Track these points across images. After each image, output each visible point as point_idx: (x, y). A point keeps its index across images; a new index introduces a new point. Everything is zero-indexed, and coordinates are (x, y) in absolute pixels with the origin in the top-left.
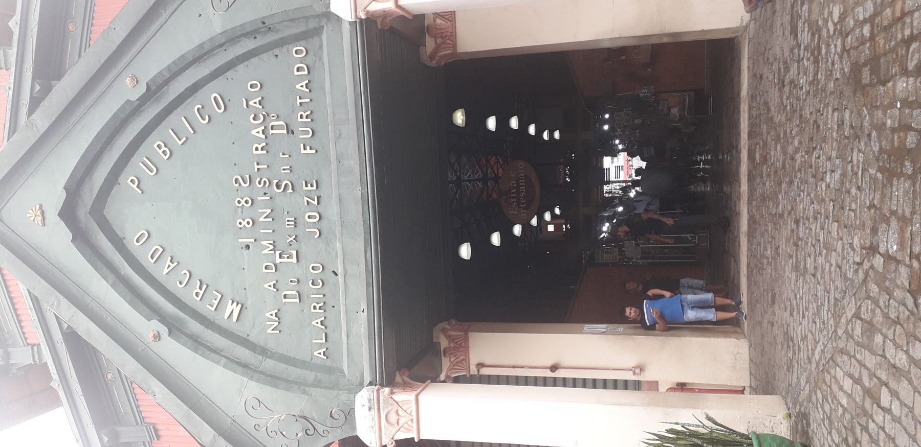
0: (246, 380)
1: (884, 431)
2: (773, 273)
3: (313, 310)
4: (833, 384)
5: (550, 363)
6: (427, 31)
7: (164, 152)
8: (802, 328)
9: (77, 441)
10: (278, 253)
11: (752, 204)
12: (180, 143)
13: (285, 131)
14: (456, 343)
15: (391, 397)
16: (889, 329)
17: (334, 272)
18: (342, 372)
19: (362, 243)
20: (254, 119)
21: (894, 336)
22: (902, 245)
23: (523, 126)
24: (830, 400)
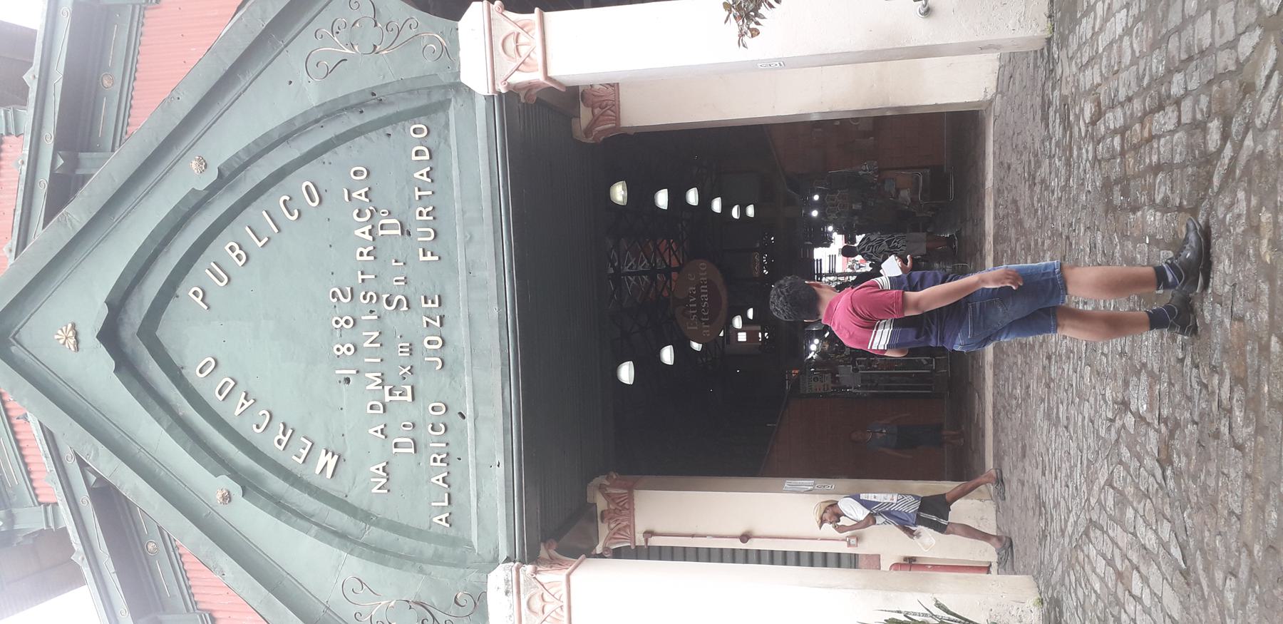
2: (1023, 418)
3: (432, 464)
4: (1086, 565)
5: (739, 531)
7: (238, 256)
10: (387, 388)
12: (260, 244)
13: (399, 232)
15: (535, 578)
16: (1139, 502)
17: (460, 413)
18: (470, 544)
20: (358, 215)
21: (1144, 511)
22: (1150, 409)
23: (705, 201)
24: (1083, 585)
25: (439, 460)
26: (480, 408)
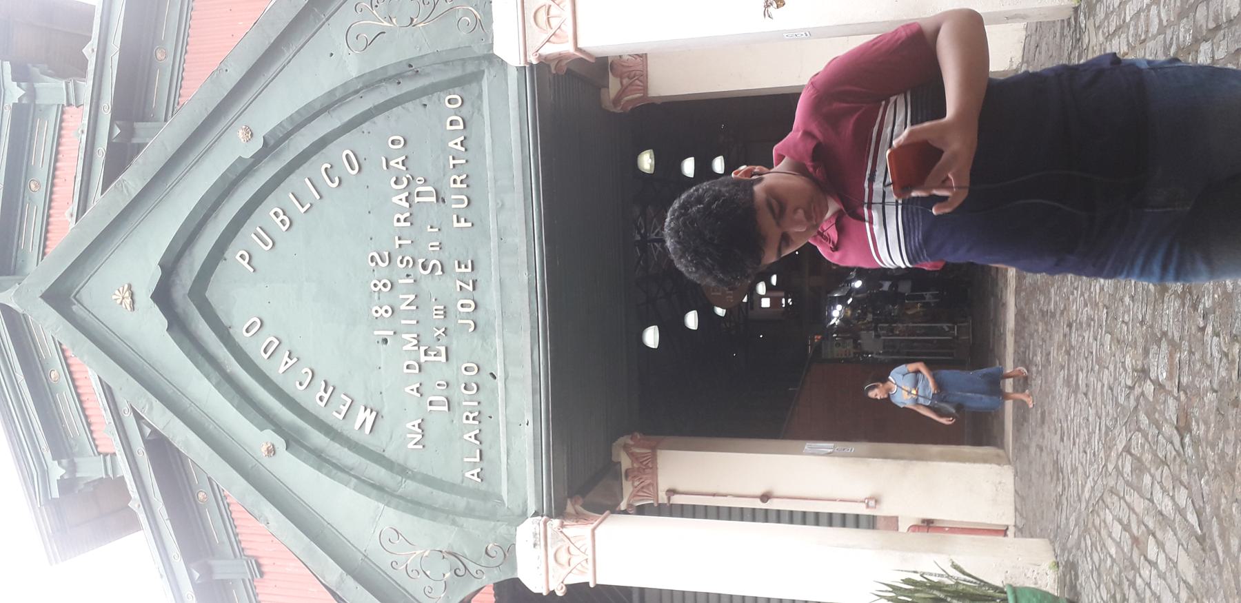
0: (382, 506)
1: (1150, 588)
3: (465, 421)
5: (760, 491)
6: (611, 70)
7: (282, 221)
8: (1072, 458)
9: (162, 576)
10: (423, 349)
11: (1020, 294)
12: (303, 210)
13: (434, 199)
14: (641, 463)
15: (561, 532)
18: (500, 498)
19: (528, 340)
20: (396, 183)
21: (1161, 478)
22: (1170, 376)
24: (1099, 549)
25: (471, 418)
26: (511, 369)
